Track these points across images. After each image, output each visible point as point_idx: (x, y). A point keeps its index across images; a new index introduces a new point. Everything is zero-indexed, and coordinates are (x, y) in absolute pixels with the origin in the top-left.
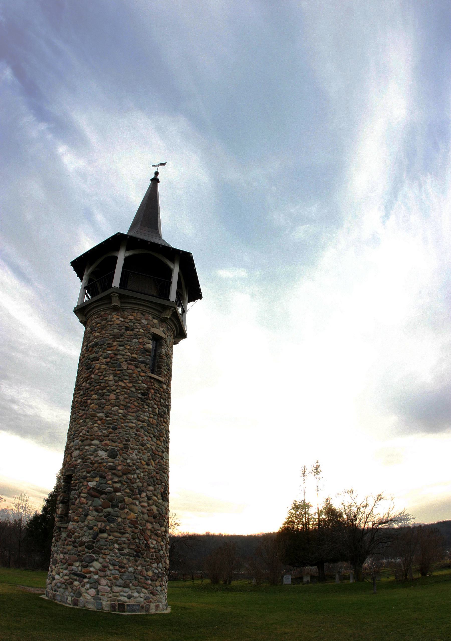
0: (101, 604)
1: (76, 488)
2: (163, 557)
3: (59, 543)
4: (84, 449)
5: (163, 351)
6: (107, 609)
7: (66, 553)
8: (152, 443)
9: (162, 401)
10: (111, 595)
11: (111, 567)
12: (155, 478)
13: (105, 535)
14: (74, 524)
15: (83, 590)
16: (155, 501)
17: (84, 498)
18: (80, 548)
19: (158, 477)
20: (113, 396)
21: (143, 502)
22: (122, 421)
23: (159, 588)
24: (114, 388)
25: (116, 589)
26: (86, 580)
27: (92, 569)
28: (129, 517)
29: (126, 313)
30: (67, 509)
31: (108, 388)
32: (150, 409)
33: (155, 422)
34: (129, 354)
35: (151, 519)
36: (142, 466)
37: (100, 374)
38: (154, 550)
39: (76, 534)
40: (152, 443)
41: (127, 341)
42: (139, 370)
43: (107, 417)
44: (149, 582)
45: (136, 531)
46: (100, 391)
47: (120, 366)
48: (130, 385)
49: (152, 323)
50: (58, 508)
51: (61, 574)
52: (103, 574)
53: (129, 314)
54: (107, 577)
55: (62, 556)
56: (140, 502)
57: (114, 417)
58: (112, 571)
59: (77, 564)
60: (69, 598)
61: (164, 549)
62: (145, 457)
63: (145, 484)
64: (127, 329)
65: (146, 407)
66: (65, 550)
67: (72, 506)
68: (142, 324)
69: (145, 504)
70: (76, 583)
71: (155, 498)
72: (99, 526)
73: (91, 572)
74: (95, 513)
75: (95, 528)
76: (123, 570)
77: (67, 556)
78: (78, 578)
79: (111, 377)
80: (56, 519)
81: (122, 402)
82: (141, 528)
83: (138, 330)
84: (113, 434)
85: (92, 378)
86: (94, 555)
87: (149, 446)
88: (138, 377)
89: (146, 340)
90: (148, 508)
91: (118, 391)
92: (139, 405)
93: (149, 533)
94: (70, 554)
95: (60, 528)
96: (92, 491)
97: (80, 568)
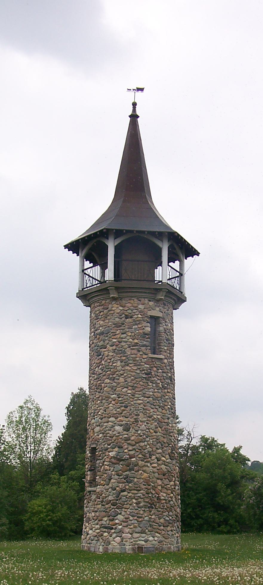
0: (125, 549)
1: (101, 458)
2: (173, 507)
3: (90, 504)
4: (103, 426)
5: (161, 328)
6: (129, 552)
7: (96, 512)
8: (158, 413)
9: (165, 375)
10: (132, 541)
11: (131, 518)
12: (162, 443)
13: (125, 493)
14: (101, 487)
15: (111, 538)
16: (164, 461)
17: (108, 465)
18: (107, 506)
19: (165, 441)
20: (122, 379)
21: (153, 463)
22: (131, 399)
23: (170, 533)
24: (122, 372)
25: (136, 535)
26: (113, 531)
27: (117, 521)
28: (143, 477)
29: (124, 302)
30: (94, 475)
31: (117, 373)
32: (154, 385)
33: (159, 395)
34: (131, 340)
35: (161, 476)
36: (150, 435)
37: (109, 361)
38: (164, 501)
39: (103, 495)
40: (158, 413)
41: (128, 328)
42: (141, 353)
43: (119, 398)
44: (162, 527)
45: (149, 487)
46: (111, 376)
47: (124, 352)
48: (136, 368)
49: (148, 306)
50: (87, 475)
51: (94, 529)
52: (125, 524)
53: (127, 302)
54: (129, 527)
55: (93, 514)
56: (151, 464)
57: (125, 397)
58: (133, 521)
59: (105, 519)
60: (101, 547)
61: (174, 500)
62: (153, 426)
63: (154, 449)
64: (127, 317)
65: (151, 384)
66: (96, 509)
67: (98, 473)
68: (139, 310)
69: (156, 465)
70: (106, 534)
71: (164, 458)
72: (120, 487)
73: (116, 524)
74: (116, 477)
75: (117, 488)
76: (140, 519)
77: (97, 514)
78: (107, 530)
79: (119, 363)
80: (86, 484)
81: (129, 384)
82: (153, 485)
83: (136, 316)
84: (125, 412)
85: (102, 364)
86: (118, 510)
87: (155, 416)
88: (141, 360)
89: (145, 324)
90: (158, 468)
91: (125, 375)
92: (144, 384)
93: (160, 488)
94: (100, 512)
95: (90, 492)
96: (113, 460)
97: (108, 522)
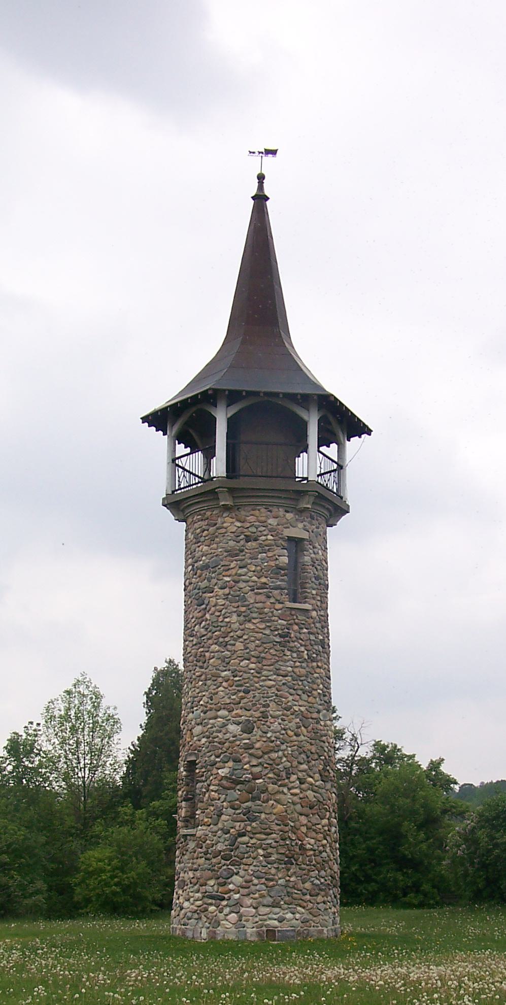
0: (245, 933)
1: (203, 778)
2: (327, 862)
3: (186, 857)
4: (207, 724)
5: (307, 559)
6: (252, 939)
7: (196, 870)
8: (301, 703)
9: (312, 637)
10: (257, 919)
11: (256, 881)
12: (309, 753)
13: (245, 839)
14: (204, 828)
15: (221, 916)
16: (312, 784)
17: (215, 791)
18: (214, 860)
19: (313, 751)
20: (239, 645)
21: (293, 788)
22: (256, 679)
23: (321, 906)
24: (239, 633)
25: (263, 910)
26: (224, 903)
27: (231, 886)
28: (275, 811)
29: (243, 513)
30: (193, 808)
31: (232, 634)
32: (295, 655)
33: (303, 671)
34: (255, 578)
35: (306, 810)
36: (288, 739)
37: (218, 614)
38: (312, 852)
39: (208, 842)
40: (301, 703)
41: (251, 558)
42: (272, 600)
43: (234, 676)
44: (308, 897)
45: (287, 829)
46: (221, 640)
47: (244, 599)
48: (263, 626)
49: (285, 521)
50: (181, 808)
51: (192, 900)
52: (245, 891)
53: (248, 514)
54: (252, 895)
55: (191, 874)
56: (289, 789)
57: (246, 676)
58: (259, 885)
59: (212, 882)
60: (204, 930)
61: (328, 850)
62: (292, 725)
63: (295, 763)
64: (248, 539)
65: (288, 653)
66: (195, 866)
67: (200, 805)
68: (270, 527)
69: (297, 791)
70: (212, 908)
71: (311, 779)
72: (237, 828)
73: (231, 891)
74: (230, 811)
75: (232, 830)
76: (271, 883)
77: (198, 874)
78: (214, 901)
79: (235, 618)
80: (179, 824)
81: (252, 653)
82: (292, 824)
83: (264, 538)
84: (245, 700)
85: (207, 620)
86: (233, 868)
87: (296, 708)
88: (272, 612)
89: (278, 551)
90: (301, 796)
91: (245, 637)
92: (277, 653)
93: (304, 829)
94: (202, 870)
95: (185, 836)
96: (224, 782)
97: (216, 887)
